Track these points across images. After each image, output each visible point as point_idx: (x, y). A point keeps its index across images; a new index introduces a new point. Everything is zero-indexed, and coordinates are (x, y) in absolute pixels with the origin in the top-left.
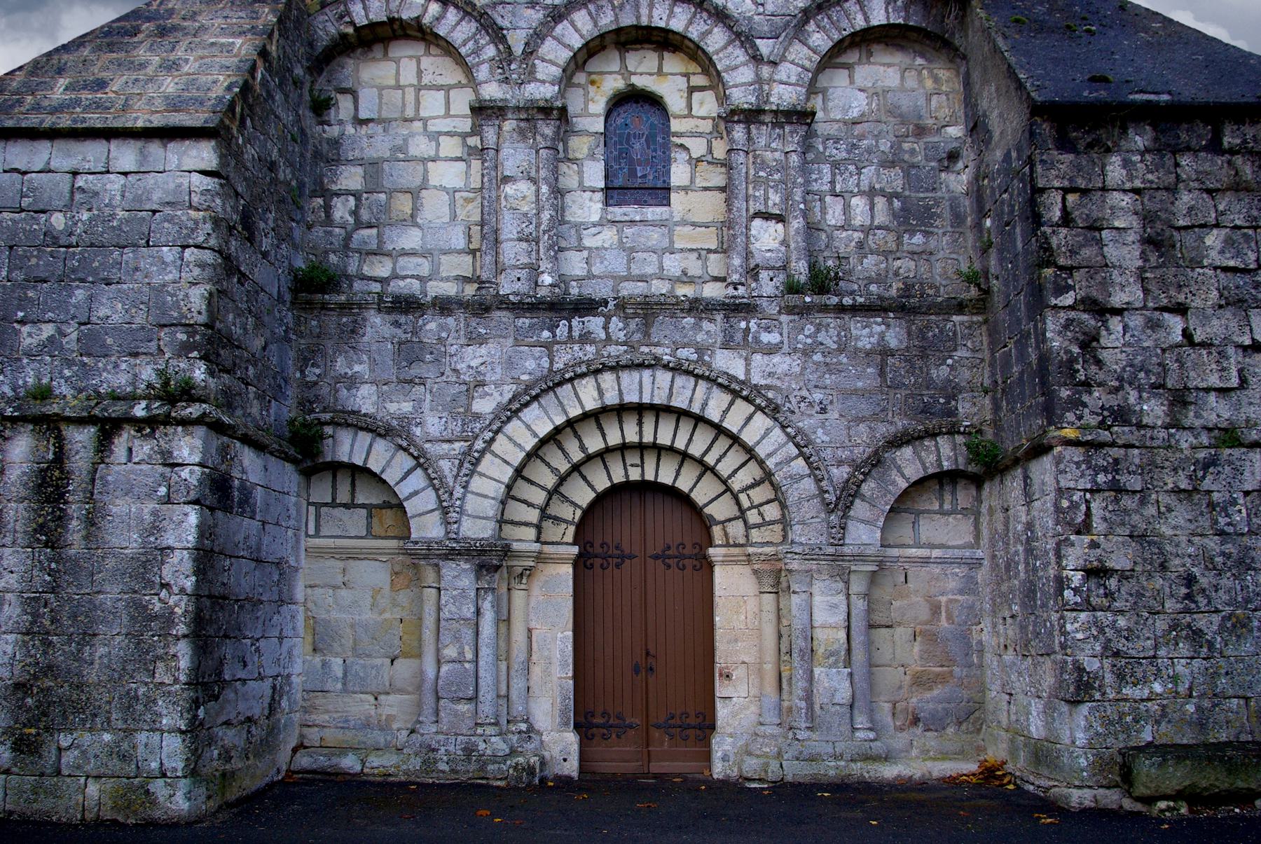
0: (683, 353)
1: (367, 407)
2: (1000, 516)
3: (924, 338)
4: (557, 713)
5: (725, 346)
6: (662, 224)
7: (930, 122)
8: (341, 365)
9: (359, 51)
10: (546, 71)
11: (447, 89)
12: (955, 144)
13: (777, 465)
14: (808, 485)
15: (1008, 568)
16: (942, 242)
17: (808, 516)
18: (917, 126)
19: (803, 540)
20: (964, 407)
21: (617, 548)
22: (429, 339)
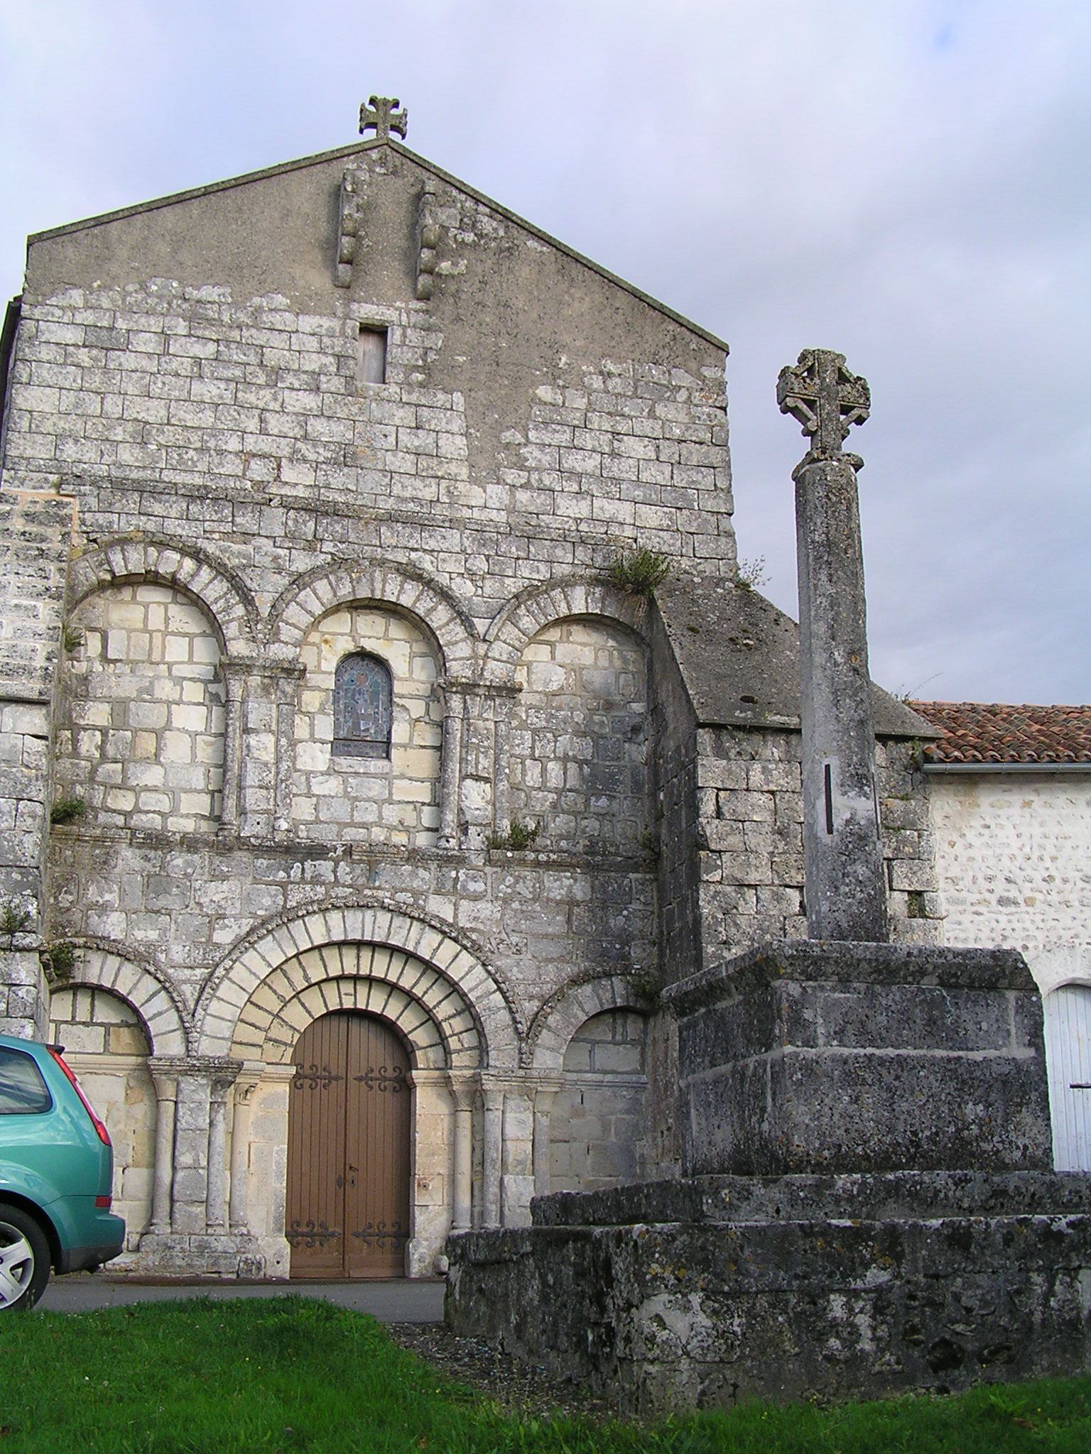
0: (401, 897)
1: (116, 934)
2: (662, 1046)
3: (605, 892)
4: (271, 1220)
5: (438, 892)
6: (384, 776)
7: (618, 698)
8: (92, 893)
9: (109, 592)
10: (287, 633)
11: (191, 637)
12: (638, 719)
13: (477, 998)
14: (504, 1016)
15: (666, 1090)
16: (623, 805)
17: (503, 1043)
18: (607, 702)
19: (498, 1064)
20: (635, 952)
21: (325, 1069)
22: (177, 874)
